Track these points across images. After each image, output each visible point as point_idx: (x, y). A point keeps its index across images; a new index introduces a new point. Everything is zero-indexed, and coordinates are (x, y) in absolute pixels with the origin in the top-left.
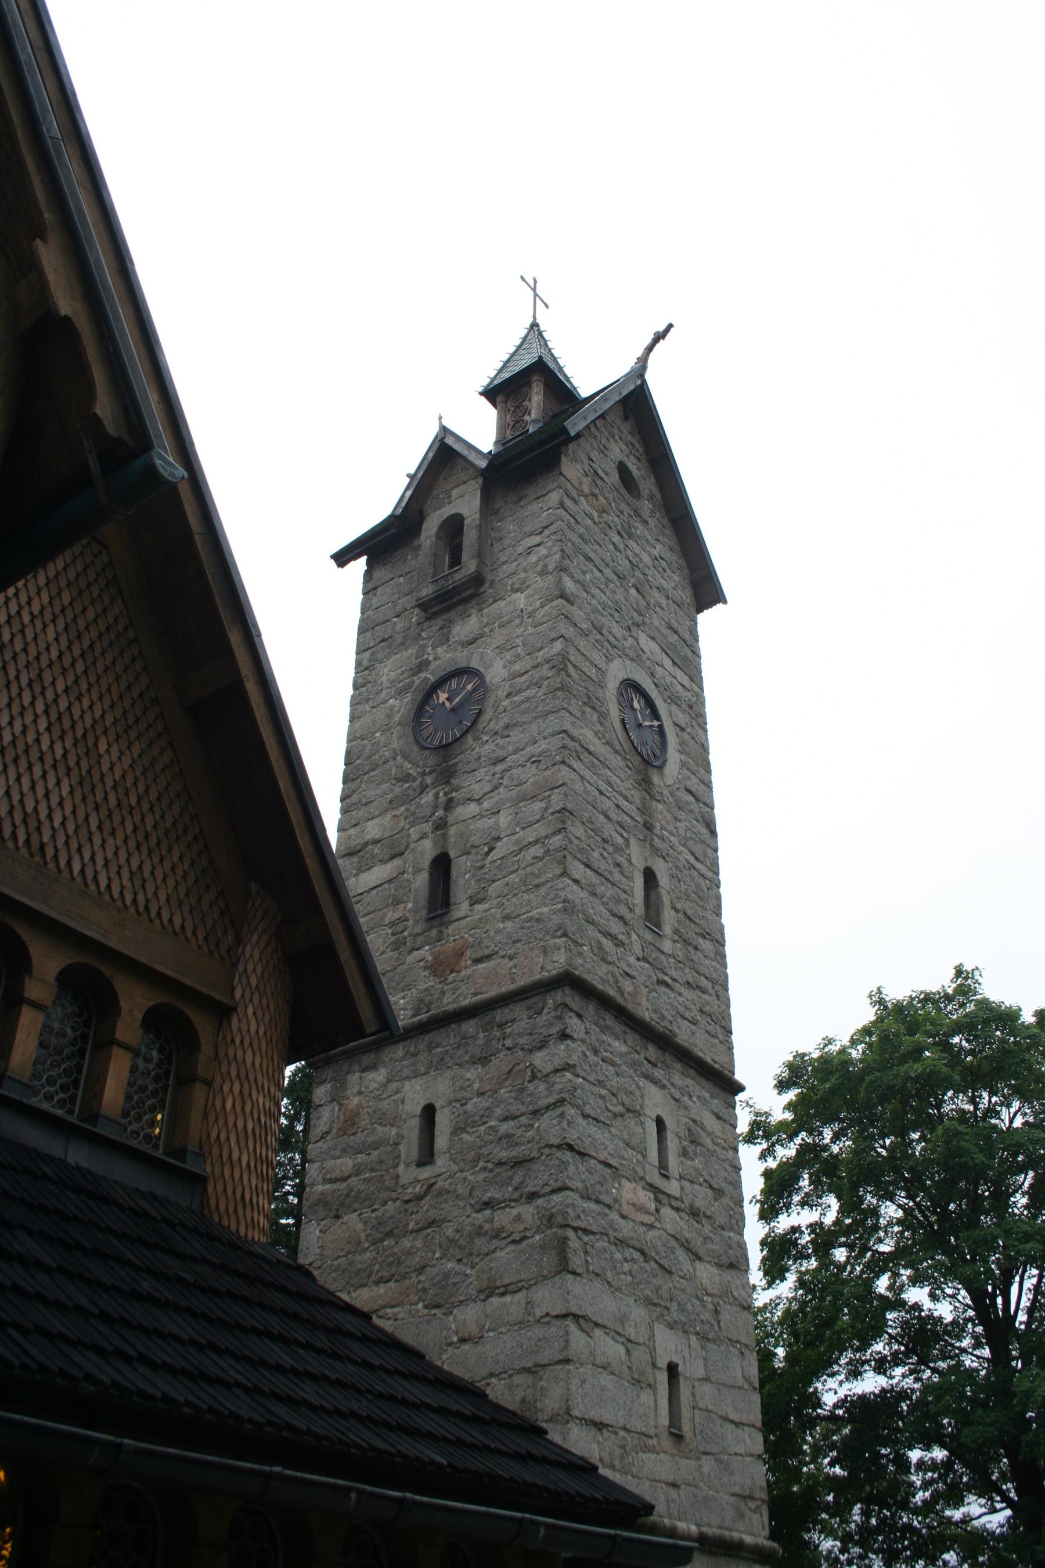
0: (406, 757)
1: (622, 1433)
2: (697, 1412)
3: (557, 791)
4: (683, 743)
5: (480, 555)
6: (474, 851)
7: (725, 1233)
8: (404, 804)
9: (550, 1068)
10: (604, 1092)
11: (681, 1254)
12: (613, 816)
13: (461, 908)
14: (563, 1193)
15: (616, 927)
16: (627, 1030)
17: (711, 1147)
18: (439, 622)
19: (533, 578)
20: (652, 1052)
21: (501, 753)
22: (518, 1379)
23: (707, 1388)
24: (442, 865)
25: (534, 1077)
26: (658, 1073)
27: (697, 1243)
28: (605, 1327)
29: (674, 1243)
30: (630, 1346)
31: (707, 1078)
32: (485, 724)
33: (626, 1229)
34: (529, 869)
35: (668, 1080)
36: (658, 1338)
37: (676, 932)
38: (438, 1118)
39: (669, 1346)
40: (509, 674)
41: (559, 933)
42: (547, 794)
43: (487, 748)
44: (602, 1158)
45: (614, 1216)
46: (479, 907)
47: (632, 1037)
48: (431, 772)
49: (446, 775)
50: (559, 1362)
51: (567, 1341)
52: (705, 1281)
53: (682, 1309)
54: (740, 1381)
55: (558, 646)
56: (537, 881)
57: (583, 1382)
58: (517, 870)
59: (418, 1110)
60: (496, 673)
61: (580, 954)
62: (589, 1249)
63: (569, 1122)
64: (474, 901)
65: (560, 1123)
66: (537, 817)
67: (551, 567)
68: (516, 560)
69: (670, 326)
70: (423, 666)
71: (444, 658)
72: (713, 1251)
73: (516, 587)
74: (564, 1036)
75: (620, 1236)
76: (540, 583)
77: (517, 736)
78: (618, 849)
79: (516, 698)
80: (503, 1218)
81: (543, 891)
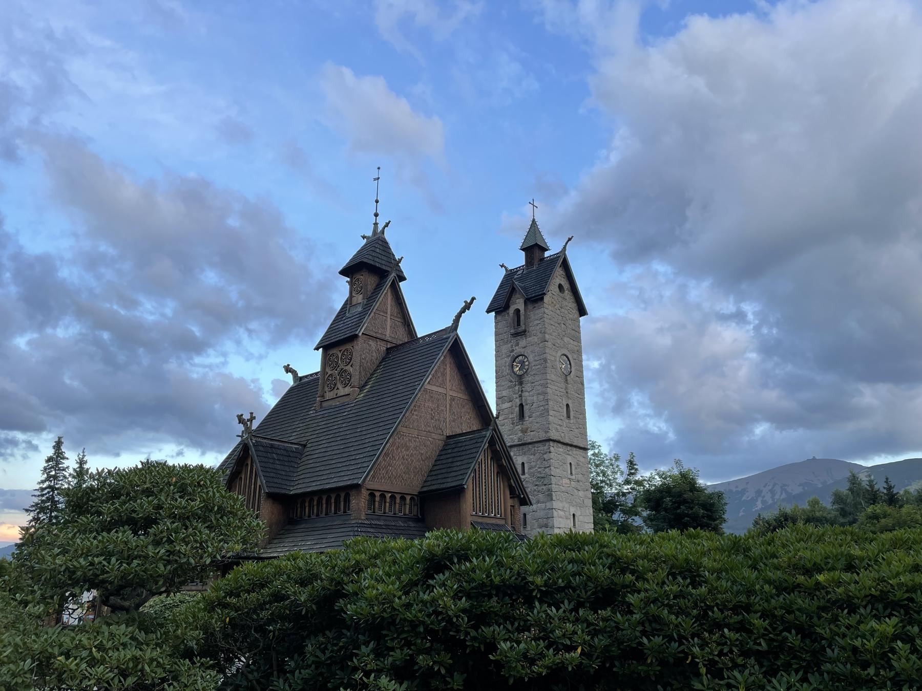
13: (527, 418)
15: (560, 422)
20: (569, 448)
24: (521, 406)
27: (579, 488)
49: (521, 383)
60: (531, 358)
70: (513, 351)
71: (518, 350)
77: (537, 378)
80: (540, 488)
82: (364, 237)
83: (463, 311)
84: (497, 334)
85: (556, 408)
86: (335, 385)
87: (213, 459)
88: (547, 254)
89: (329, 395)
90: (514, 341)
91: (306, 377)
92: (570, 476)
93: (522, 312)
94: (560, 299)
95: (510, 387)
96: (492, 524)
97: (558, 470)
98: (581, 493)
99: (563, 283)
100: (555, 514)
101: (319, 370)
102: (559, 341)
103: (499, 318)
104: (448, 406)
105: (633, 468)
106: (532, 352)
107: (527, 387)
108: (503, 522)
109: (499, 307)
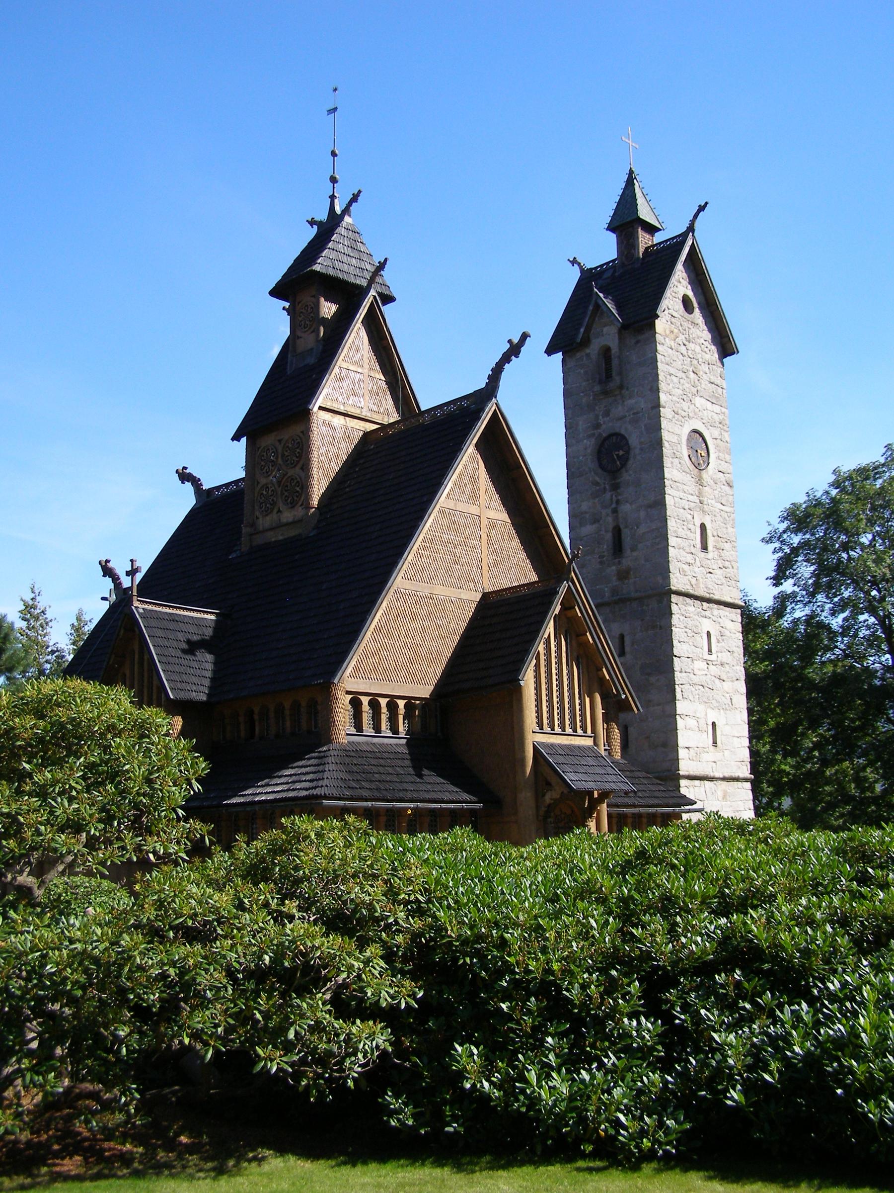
4: (717, 446)
11: (717, 681)
13: (627, 552)
15: (689, 559)
24: (617, 533)
27: (724, 677)
33: (695, 679)
38: (626, 639)
49: (615, 487)
54: (740, 722)
59: (617, 636)
64: (633, 550)
71: (607, 426)
80: (653, 679)
82: (312, 223)
83: (506, 358)
84: (567, 394)
85: (681, 533)
86: (274, 504)
87: (172, 697)
89: (264, 522)
91: (218, 488)
93: (615, 350)
95: (595, 495)
97: (684, 647)
98: (727, 686)
101: (242, 474)
102: (685, 405)
103: (571, 363)
104: (484, 536)
108: (589, 742)
109: (564, 341)
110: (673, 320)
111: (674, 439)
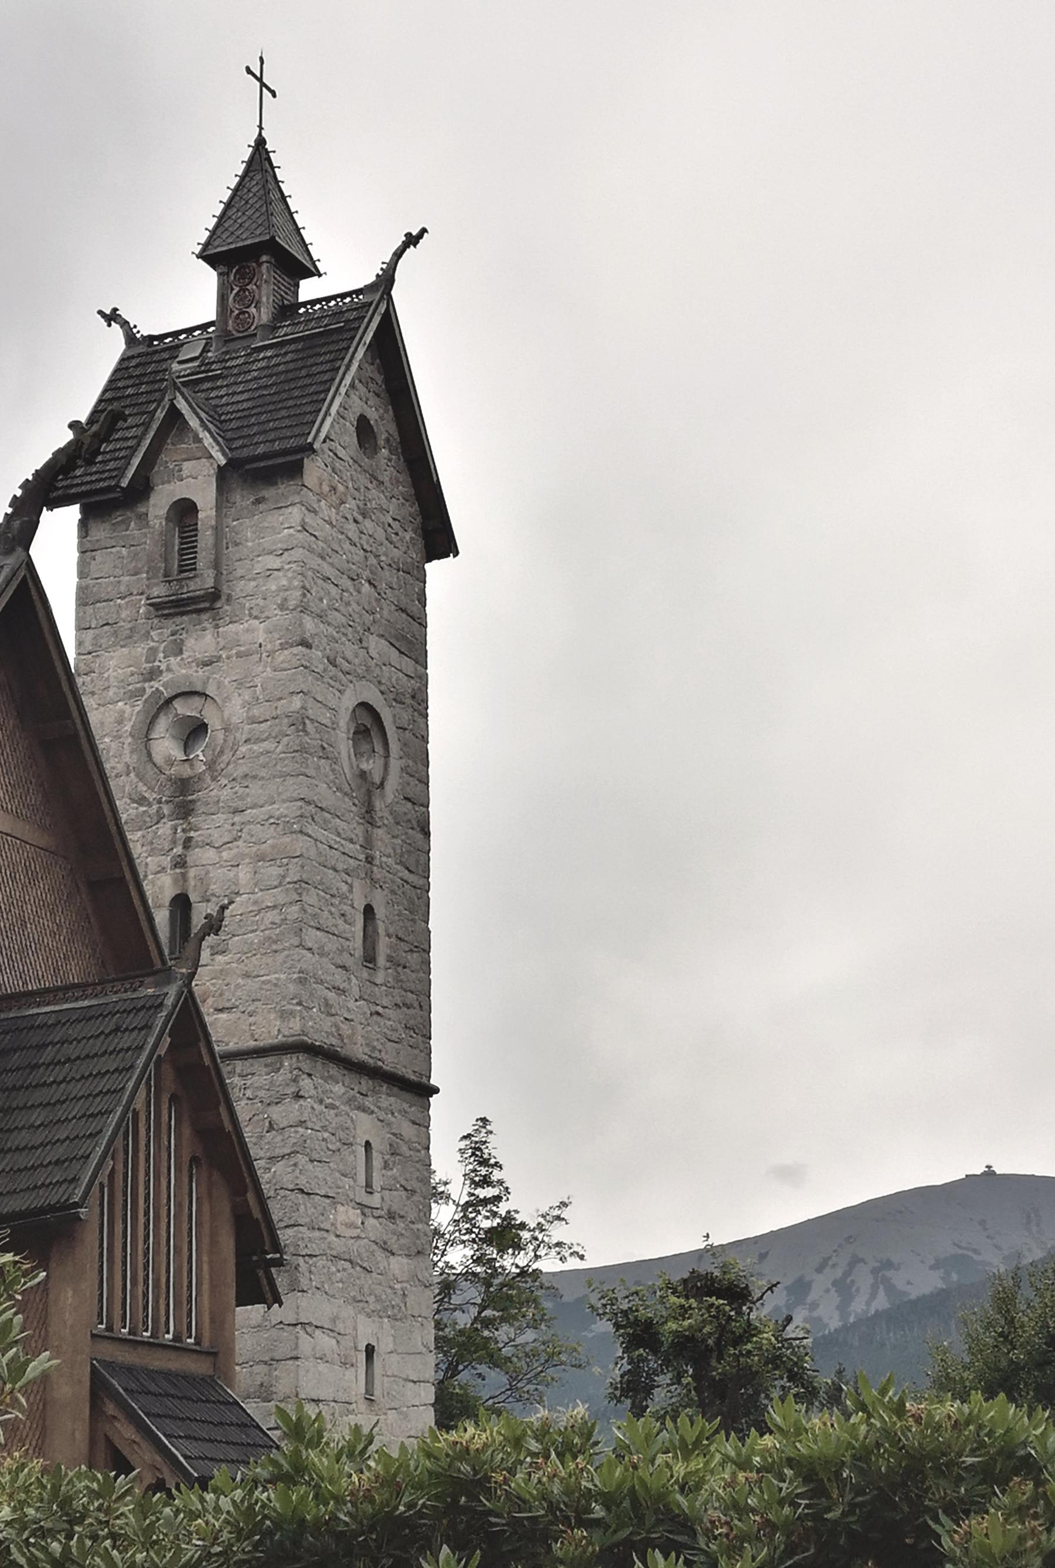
0: (141, 778)
1: (333, 1404)
2: (385, 1378)
3: (296, 860)
5: (216, 565)
6: (214, 899)
7: (415, 1227)
8: (140, 829)
9: (285, 1124)
10: (326, 1135)
11: (380, 1254)
12: (340, 866)
14: (296, 1228)
15: (338, 978)
16: (346, 1072)
17: (408, 1153)
18: (170, 625)
19: (273, 610)
20: (366, 1084)
21: (240, 805)
22: (257, 1369)
23: (394, 1358)
25: (271, 1128)
26: (368, 1102)
27: (393, 1244)
28: (322, 1328)
29: (375, 1247)
30: (339, 1338)
31: (408, 1091)
32: (222, 766)
34: (267, 932)
35: (375, 1105)
36: (360, 1328)
37: (390, 959)
39: (366, 1331)
40: (248, 718)
41: (294, 1002)
42: (285, 861)
43: (225, 793)
44: (323, 1193)
45: (332, 1238)
46: (219, 958)
47: (349, 1078)
48: (167, 802)
49: (185, 811)
50: (292, 1358)
51: (297, 1344)
52: (397, 1272)
53: (378, 1299)
55: (297, 703)
56: (274, 947)
57: (308, 1371)
58: (256, 930)
61: (311, 1018)
62: (313, 1268)
63: (301, 1170)
65: (293, 1171)
66: (276, 883)
67: (292, 603)
68: (254, 579)
69: (424, 231)
70: (153, 674)
71: (177, 671)
72: (404, 1245)
73: (255, 613)
74: (298, 1096)
75: (334, 1253)
76: (279, 618)
77: (255, 790)
78: (343, 897)
79: (255, 747)
81: (280, 957)
88: (309, 290)
90: (161, 634)
92: (363, 1197)
93: (207, 513)
94: (363, 480)
96: (167, 1375)
97: (318, 1170)
99: (372, 415)
100: (306, 1343)
103: (100, 532)
105: (486, 1182)
106: (240, 684)
107: (212, 826)
110: (338, 464)
111: (326, 718)
